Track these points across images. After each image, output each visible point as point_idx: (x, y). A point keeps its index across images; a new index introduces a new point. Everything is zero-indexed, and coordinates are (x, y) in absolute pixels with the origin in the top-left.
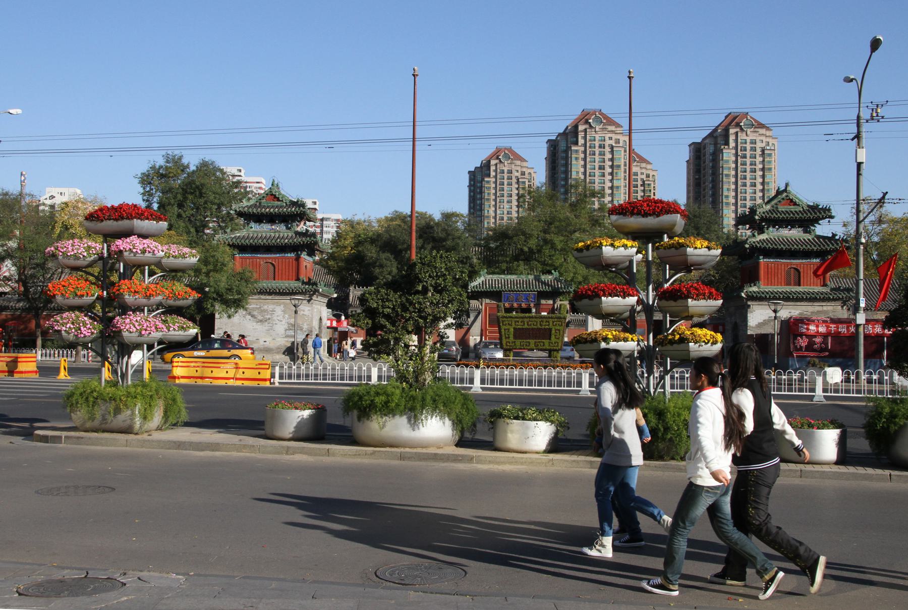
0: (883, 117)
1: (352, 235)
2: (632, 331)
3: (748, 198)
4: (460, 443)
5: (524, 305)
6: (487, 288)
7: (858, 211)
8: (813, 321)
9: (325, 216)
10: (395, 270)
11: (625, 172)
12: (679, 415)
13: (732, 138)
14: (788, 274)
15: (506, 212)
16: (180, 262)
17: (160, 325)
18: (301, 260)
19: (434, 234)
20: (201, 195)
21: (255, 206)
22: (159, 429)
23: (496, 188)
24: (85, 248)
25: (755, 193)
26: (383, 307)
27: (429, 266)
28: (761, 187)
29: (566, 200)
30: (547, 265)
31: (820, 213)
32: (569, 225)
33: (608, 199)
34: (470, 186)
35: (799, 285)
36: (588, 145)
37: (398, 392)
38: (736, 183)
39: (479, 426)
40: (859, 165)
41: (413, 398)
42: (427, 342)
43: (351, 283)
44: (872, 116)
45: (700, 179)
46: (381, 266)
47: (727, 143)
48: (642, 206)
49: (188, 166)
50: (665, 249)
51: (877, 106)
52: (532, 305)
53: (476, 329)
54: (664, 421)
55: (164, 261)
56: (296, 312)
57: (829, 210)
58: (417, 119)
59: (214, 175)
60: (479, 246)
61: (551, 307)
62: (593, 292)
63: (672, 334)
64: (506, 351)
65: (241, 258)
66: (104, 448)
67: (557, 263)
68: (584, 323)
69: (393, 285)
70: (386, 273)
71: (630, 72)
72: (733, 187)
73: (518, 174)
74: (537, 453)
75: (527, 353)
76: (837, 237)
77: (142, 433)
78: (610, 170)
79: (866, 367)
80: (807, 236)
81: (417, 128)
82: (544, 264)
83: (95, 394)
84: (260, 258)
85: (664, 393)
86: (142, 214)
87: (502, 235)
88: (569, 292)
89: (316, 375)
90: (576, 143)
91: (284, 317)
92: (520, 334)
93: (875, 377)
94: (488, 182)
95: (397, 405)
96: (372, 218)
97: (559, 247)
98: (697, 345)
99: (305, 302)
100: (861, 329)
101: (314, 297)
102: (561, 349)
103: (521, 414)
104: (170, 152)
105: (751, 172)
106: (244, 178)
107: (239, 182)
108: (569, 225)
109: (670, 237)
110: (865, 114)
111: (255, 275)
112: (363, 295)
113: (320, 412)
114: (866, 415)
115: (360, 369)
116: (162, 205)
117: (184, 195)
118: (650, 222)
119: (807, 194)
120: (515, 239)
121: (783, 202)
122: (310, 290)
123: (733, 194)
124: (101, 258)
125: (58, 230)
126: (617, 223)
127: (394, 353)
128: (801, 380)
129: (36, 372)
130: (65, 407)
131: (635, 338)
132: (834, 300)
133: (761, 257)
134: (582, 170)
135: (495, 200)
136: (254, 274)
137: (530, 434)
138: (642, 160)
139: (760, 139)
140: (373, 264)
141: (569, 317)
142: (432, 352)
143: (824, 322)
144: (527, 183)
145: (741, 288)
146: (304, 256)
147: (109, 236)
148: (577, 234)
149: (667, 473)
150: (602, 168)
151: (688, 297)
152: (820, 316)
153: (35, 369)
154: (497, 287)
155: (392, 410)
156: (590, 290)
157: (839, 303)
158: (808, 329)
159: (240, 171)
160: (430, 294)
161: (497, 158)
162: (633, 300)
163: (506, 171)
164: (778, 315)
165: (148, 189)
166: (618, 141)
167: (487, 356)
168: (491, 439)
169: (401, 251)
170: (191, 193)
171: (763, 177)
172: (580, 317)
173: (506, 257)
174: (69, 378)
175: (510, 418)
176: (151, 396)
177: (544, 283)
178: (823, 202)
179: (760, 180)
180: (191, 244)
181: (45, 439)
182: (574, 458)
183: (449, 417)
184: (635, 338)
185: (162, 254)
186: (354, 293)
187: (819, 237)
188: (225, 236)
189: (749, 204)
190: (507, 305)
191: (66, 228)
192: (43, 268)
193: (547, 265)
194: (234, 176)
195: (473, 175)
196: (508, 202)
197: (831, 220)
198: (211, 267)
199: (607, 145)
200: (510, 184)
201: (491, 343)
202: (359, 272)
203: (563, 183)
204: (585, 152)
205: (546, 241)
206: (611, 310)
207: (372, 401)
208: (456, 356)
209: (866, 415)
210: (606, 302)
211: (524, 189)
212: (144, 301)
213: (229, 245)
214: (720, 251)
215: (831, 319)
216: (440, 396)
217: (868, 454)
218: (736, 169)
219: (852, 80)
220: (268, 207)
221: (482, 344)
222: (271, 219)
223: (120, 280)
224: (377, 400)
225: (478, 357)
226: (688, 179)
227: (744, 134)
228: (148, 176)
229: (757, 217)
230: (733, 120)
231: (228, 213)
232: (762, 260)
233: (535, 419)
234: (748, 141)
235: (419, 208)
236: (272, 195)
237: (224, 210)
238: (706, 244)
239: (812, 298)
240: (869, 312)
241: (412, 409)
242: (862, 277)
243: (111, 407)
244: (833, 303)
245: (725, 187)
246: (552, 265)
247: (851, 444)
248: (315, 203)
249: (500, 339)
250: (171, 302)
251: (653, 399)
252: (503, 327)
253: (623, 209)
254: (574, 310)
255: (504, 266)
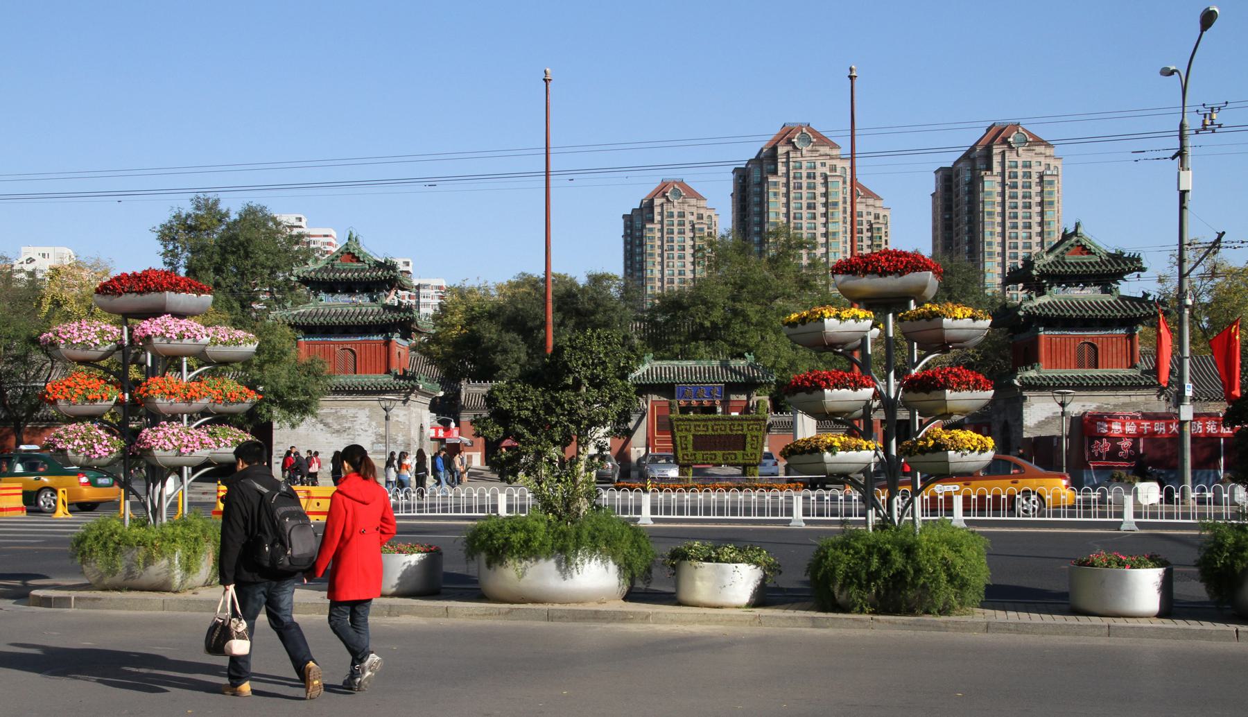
0: (1220, 126)
1: (463, 308)
2: (867, 435)
3: (1020, 245)
4: (630, 596)
5: (706, 403)
6: (653, 380)
7: (1181, 261)
8: (1117, 417)
9: (422, 282)
10: (524, 357)
11: (845, 212)
12: (935, 551)
13: (996, 160)
14: (1080, 351)
15: (676, 272)
16: (231, 350)
17: (207, 439)
18: (392, 344)
19: (578, 306)
20: (247, 255)
21: (325, 269)
22: (207, 584)
23: (662, 238)
24: (96, 333)
25: (1030, 238)
26: (519, 409)
27: (581, 350)
28: (1039, 229)
29: (761, 253)
30: (737, 345)
31: (1124, 264)
32: (768, 288)
33: (820, 251)
34: (625, 236)
35: (1096, 367)
36: (792, 175)
37: (542, 526)
38: (1003, 224)
39: (655, 571)
40: (1183, 194)
41: (564, 535)
42: (581, 457)
43: (462, 376)
44: (1204, 125)
45: (951, 219)
46: (505, 351)
47: (989, 168)
48: (878, 261)
49: (227, 214)
50: (911, 320)
51: (1212, 109)
52: (718, 402)
53: (639, 437)
54: (914, 560)
55: (209, 349)
56: (387, 418)
57: (1139, 260)
58: (551, 144)
59: (265, 225)
60: (642, 320)
61: (744, 405)
62: (812, 382)
63: (923, 439)
64: (683, 468)
65: (306, 343)
66: (131, 612)
67: (752, 344)
68: (792, 427)
69: (530, 378)
70: (511, 361)
71: (851, 70)
72: (999, 229)
73: (694, 218)
74: (738, 607)
75: (715, 470)
76: (1150, 298)
77: (185, 591)
78: (823, 210)
79: (1195, 481)
80: (1107, 298)
81: (551, 157)
82: (733, 344)
83: (116, 538)
84: (334, 343)
85: (913, 521)
86: (177, 284)
87: (674, 305)
88: (770, 383)
89: (433, 505)
90: (775, 172)
91: (370, 425)
92: (702, 443)
93: (1209, 495)
94: (651, 230)
95: (542, 544)
96: (490, 284)
97: (754, 320)
98: (959, 454)
99: (399, 403)
100: (1187, 428)
101: (412, 397)
102: (760, 464)
103: (714, 555)
104: (201, 195)
105: (1025, 207)
106: (306, 230)
107: (301, 236)
108: (768, 288)
109: (919, 304)
110: (1193, 122)
111: (328, 368)
112: (491, 392)
113: (434, 557)
114: (1200, 547)
115: (482, 496)
116: (191, 271)
117: (222, 255)
118: (891, 283)
119: (1106, 238)
120: (692, 310)
121: (1072, 249)
122: (406, 386)
123: (999, 239)
124: (120, 347)
125: (46, 308)
126: (844, 286)
127: (536, 472)
128: (1102, 501)
129: (22, 509)
130: (73, 557)
131: (872, 446)
132: (1147, 387)
133: (1041, 329)
134: (784, 210)
135: (662, 255)
136: (327, 366)
137: (727, 581)
138: (869, 194)
139: (1037, 160)
140: (493, 350)
141: (771, 418)
142: (588, 470)
143: (1133, 418)
144: (706, 230)
145: (1013, 373)
146: (396, 338)
147: (127, 316)
148: (779, 302)
149: (919, 633)
150: (811, 206)
151: (944, 387)
152: (1127, 412)
153: (21, 504)
154: (667, 378)
155: (535, 551)
156: (807, 379)
157: (1154, 391)
158: (1110, 429)
159: (300, 219)
160: (584, 389)
161: (664, 195)
162: (867, 393)
163: (676, 214)
164: (1067, 409)
165: (171, 247)
166: (833, 168)
167: (657, 474)
168: (673, 590)
169: (531, 330)
170: (233, 253)
171: (1042, 214)
172: (785, 417)
173: (680, 335)
174: (70, 516)
175: (698, 559)
176: (196, 539)
177: (733, 371)
178: (1129, 249)
179: (1036, 219)
180: (237, 324)
181: (46, 602)
182: (790, 613)
183: (613, 559)
184: (872, 446)
185: (206, 340)
186: (472, 391)
187: (1123, 298)
188: (285, 313)
189: (1021, 253)
190: (682, 403)
191: (57, 304)
192: (25, 363)
193: (737, 345)
194: (292, 227)
195: (629, 220)
196: (680, 257)
197: (1142, 274)
198: (265, 357)
199: (818, 175)
200: (682, 232)
201: (661, 457)
202: (473, 361)
203: (757, 229)
204: (787, 185)
205: (735, 313)
206: (837, 406)
207: (506, 539)
208: (613, 475)
209: (1200, 547)
210: (831, 397)
211: (701, 238)
212: (182, 406)
213: (290, 325)
214: (989, 321)
215: (1143, 414)
216: (600, 531)
217: (1205, 603)
218: (1003, 203)
219: (1172, 73)
220: (344, 271)
221: (649, 459)
222: (349, 287)
223: (147, 378)
224: (514, 537)
225: (643, 476)
226: (934, 220)
227: (1014, 153)
228: (170, 228)
229: (1034, 272)
230: (999, 135)
231: (287, 280)
232: (1043, 333)
233: (734, 561)
234: (1020, 164)
235: (556, 269)
236: (350, 254)
237: (281, 277)
238: (969, 312)
239: (1115, 386)
240: (1197, 403)
241: (563, 550)
242: (1187, 353)
243: (140, 554)
244: (1145, 392)
245: (987, 231)
246: (744, 346)
247: (1179, 589)
248: (407, 264)
249: (675, 450)
250: (220, 407)
251: (897, 529)
252: (678, 434)
253: (852, 266)
254: (777, 407)
255: (677, 348)
